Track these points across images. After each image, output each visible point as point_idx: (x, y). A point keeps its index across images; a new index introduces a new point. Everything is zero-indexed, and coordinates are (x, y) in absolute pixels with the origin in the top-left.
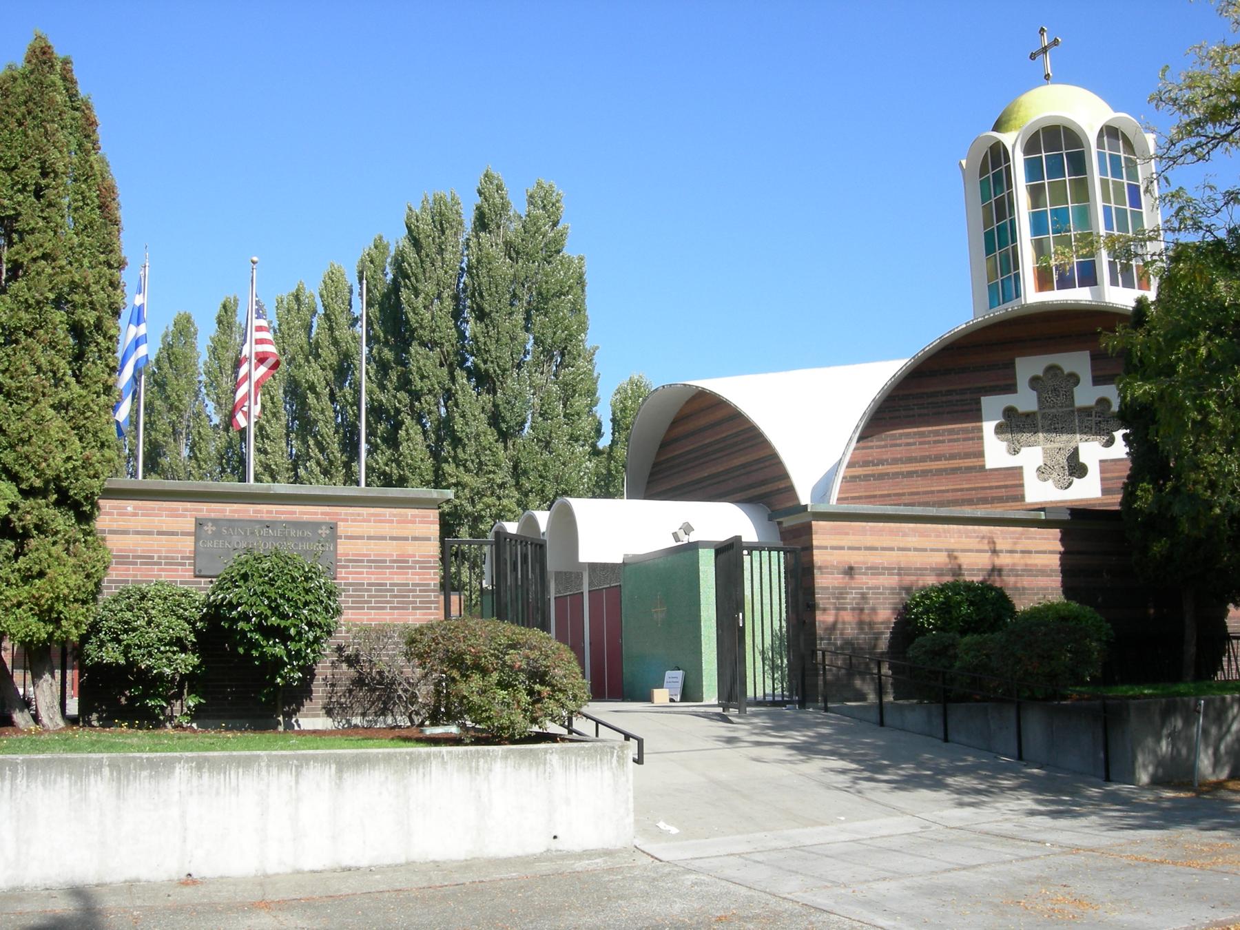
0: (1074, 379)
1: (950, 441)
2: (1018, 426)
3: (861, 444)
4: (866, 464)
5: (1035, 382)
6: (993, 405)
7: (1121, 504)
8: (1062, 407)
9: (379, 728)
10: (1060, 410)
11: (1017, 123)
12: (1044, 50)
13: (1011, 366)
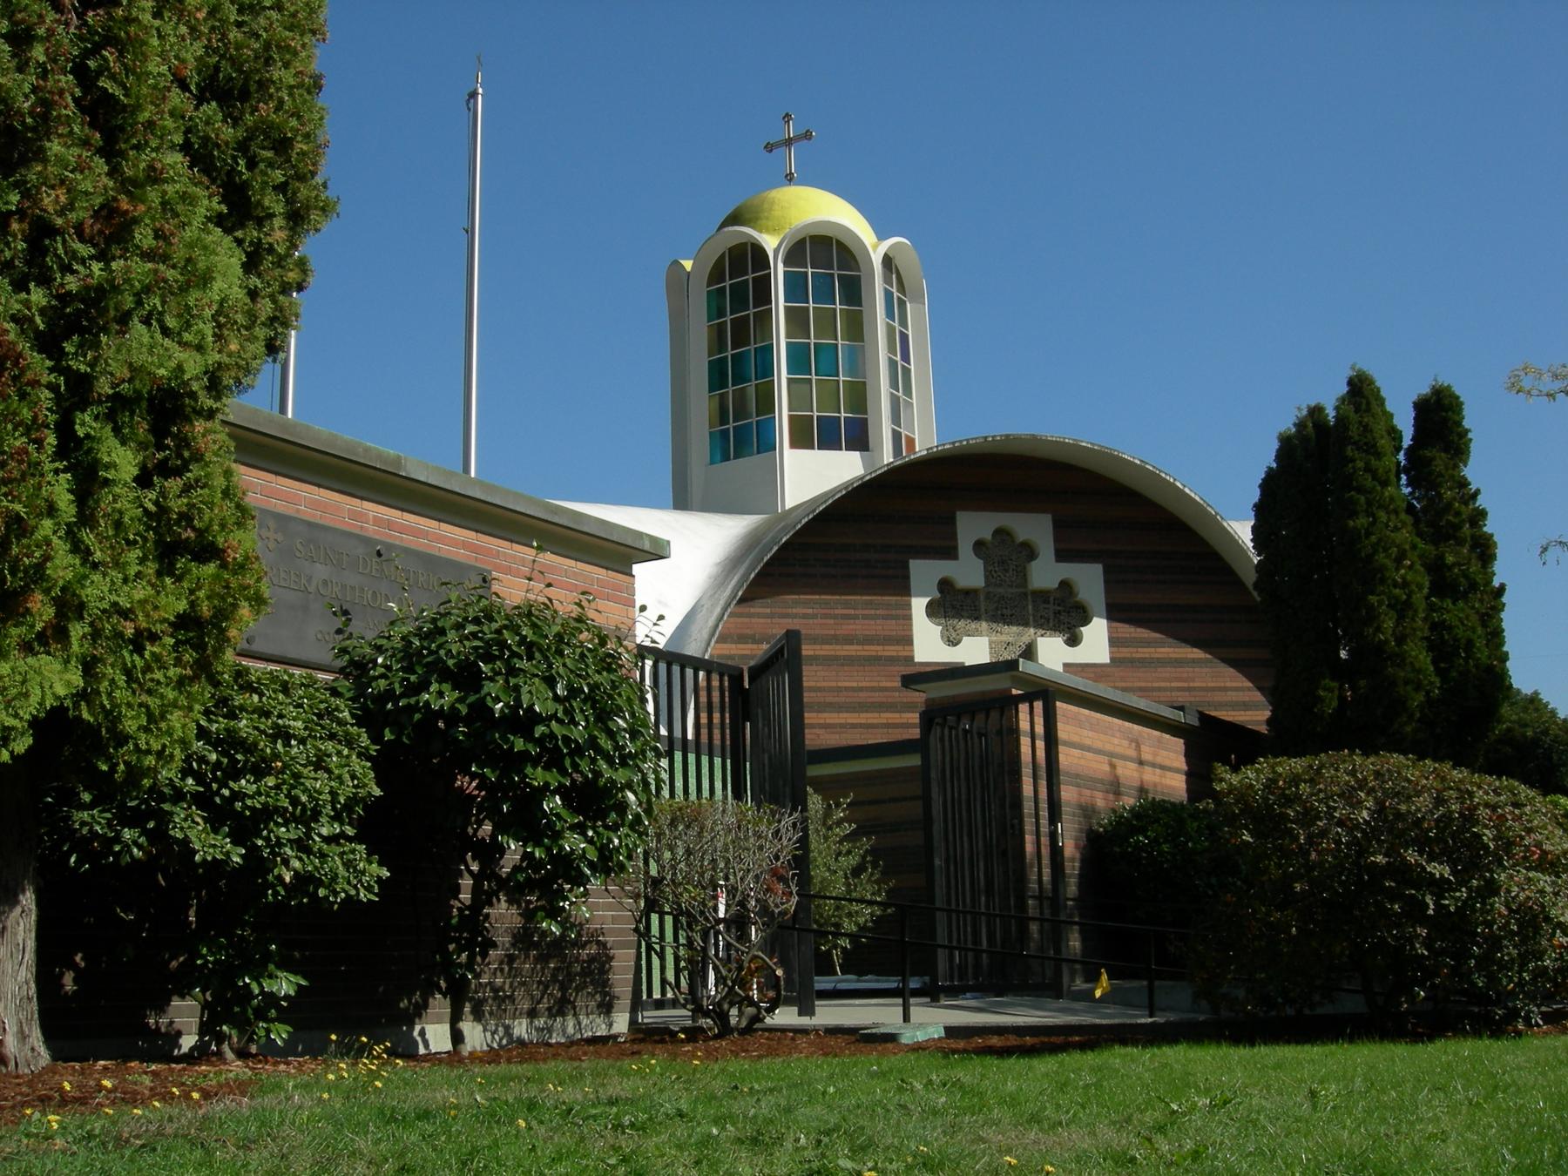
0: (1029, 551)
1: (865, 617)
2: (953, 607)
3: (742, 609)
4: (742, 639)
5: (979, 546)
6: (925, 572)
7: (1269, 722)
8: (1011, 586)
9: (557, 1043)
10: (1010, 590)
11: (770, 223)
12: (789, 142)
13: (951, 521)
